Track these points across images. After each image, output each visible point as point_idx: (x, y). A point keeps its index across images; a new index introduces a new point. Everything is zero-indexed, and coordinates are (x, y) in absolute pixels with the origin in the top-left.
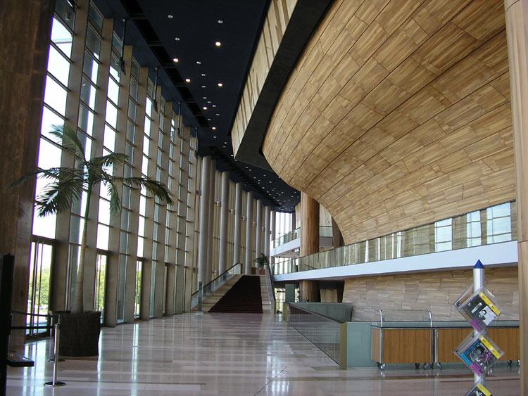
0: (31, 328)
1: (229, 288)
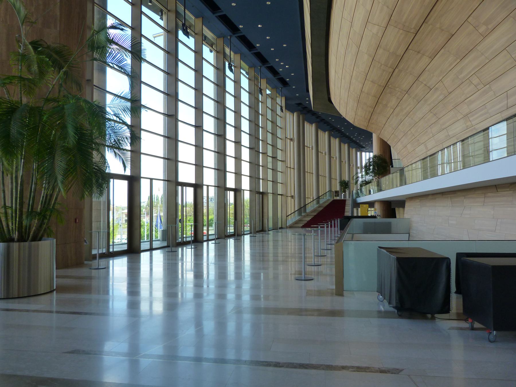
0: (186, 237)
1: (321, 209)
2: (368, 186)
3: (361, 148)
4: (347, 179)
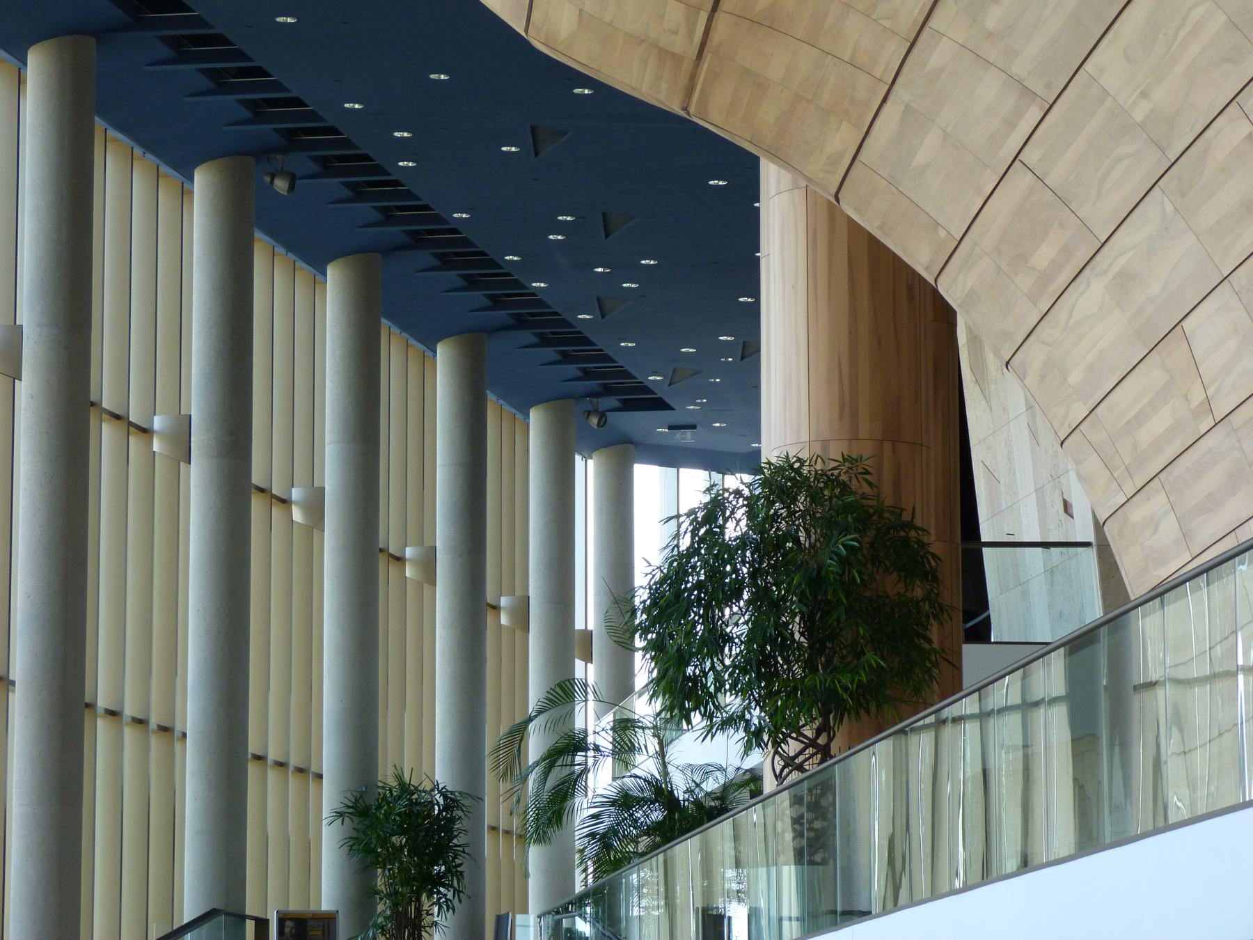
2: (687, 850)
3: (615, 405)
4: (440, 771)
